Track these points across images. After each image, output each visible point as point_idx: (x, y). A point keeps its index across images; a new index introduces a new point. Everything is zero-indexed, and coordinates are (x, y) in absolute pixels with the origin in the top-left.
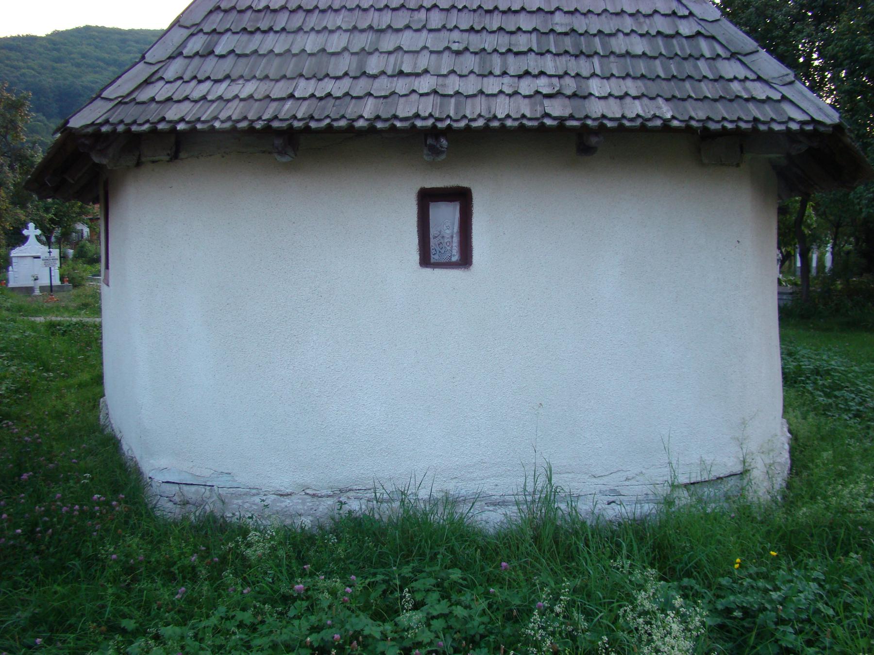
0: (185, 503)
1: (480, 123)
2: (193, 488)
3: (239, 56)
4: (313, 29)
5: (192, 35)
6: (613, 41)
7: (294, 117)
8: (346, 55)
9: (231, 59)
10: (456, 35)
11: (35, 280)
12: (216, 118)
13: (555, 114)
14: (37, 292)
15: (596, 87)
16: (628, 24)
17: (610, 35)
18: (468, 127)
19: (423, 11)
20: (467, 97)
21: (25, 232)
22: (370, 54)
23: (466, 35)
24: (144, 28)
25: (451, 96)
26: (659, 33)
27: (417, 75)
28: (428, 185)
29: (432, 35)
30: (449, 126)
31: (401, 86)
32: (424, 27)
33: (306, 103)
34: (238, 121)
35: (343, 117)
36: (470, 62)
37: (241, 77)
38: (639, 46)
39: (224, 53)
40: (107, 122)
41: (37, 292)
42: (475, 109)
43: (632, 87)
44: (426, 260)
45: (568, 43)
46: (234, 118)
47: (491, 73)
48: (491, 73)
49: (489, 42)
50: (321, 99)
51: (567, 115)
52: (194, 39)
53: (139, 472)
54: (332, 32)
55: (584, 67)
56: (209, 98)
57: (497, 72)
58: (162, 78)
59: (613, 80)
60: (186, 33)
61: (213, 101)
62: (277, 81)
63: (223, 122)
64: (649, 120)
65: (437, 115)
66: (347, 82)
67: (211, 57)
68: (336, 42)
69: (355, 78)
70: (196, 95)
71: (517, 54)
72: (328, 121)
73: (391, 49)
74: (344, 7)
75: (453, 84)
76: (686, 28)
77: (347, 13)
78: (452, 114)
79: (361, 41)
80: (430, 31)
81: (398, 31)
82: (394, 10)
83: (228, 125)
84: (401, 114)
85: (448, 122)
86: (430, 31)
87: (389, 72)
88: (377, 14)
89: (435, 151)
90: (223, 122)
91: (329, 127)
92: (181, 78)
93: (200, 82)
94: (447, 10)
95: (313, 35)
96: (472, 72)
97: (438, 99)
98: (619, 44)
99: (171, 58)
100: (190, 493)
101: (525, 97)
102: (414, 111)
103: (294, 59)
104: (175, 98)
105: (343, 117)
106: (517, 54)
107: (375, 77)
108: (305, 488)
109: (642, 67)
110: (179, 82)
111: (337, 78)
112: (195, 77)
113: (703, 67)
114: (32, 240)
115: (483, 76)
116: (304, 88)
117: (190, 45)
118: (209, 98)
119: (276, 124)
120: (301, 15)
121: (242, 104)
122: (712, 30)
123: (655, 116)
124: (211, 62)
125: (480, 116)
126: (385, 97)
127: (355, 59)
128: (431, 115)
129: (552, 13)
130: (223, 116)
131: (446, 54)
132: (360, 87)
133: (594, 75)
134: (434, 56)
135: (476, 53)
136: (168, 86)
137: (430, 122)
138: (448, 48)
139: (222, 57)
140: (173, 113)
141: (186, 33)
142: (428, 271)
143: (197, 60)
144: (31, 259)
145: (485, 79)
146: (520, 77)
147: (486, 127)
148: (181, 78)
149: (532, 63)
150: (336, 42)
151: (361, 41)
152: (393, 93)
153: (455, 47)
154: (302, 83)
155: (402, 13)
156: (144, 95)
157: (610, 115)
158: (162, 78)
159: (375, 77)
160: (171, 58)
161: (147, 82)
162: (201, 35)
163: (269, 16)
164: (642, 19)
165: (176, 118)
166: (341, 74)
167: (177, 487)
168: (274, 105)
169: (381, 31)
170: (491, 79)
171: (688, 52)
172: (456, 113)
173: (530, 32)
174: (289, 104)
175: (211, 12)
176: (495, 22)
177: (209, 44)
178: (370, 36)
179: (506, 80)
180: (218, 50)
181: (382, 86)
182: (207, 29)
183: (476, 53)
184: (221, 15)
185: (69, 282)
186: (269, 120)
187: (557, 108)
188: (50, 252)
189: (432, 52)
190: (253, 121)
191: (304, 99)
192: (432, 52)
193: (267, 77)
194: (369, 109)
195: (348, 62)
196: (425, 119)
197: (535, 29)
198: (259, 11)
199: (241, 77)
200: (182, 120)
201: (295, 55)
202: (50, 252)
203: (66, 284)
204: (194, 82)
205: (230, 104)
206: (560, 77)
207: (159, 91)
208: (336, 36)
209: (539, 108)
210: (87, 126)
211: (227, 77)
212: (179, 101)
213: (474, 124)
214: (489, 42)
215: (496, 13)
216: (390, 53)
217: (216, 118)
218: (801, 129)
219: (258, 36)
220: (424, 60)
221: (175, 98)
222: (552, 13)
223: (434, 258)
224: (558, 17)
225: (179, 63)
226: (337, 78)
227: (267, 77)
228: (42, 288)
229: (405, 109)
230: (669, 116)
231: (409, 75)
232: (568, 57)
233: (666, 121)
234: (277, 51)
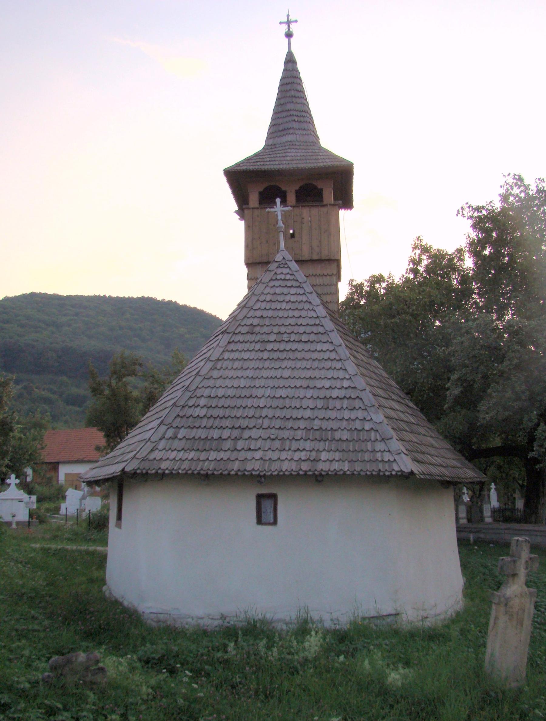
0: (159, 621)
1: (276, 473)
2: (162, 615)
3: (187, 439)
4: (217, 427)
5: (168, 428)
6: (336, 433)
7: (209, 469)
8: (229, 440)
9: (184, 441)
10: (273, 431)
11: (13, 516)
12: (180, 469)
13: (304, 469)
14: (14, 526)
15: (324, 456)
16: (344, 424)
17: (335, 430)
18: (271, 474)
19: (261, 419)
20: (274, 461)
21: (8, 481)
22: (239, 439)
23: (277, 430)
24: (74, 294)
25: (267, 460)
26: (356, 429)
27: (256, 450)
28: (260, 492)
29: (264, 431)
30: (265, 474)
31: (249, 455)
32: (261, 427)
33: (213, 462)
34: (188, 470)
35: (226, 470)
36: (277, 444)
37: (189, 449)
38: (345, 435)
39: (181, 438)
40: (139, 468)
41: (14, 526)
42: (275, 466)
43: (337, 456)
44: (260, 521)
45: (317, 435)
46: (187, 469)
47: (284, 449)
48: (284, 449)
49: (286, 434)
50: (219, 461)
51: (308, 470)
52: (169, 430)
53: (136, 611)
54: (224, 428)
55: (321, 446)
56: (177, 459)
57: (287, 449)
58: (157, 449)
59: (331, 452)
60: (166, 427)
61: (178, 461)
62: (202, 451)
63: (182, 470)
64: (338, 471)
65: (261, 470)
66: (229, 453)
67: (176, 439)
68: (226, 434)
69: (232, 451)
70: (171, 457)
71: (297, 440)
72: (221, 471)
73: (247, 438)
74: (230, 416)
75: (270, 454)
76: (367, 426)
77: (231, 419)
78: (266, 469)
79: (236, 433)
80: (264, 429)
81: (250, 428)
82: (250, 418)
83: (184, 472)
84: (248, 469)
85: (264, 472)
86: (264, 429)
87: (245, 449)
88: (243, 420)
89: (260, 482)
90: (182, 470)
91: (221, 474)
92: (165, 449)
93: (172, 451)
94: (271, 418)
95: (216, 429)
96: (277, 449)
97: (262, 462)
98: (338, 435)
99: (160, 439)
100: (161, 617)
101: (295, 461)
102: (252, 468)
103: (209, 441)
104: (164, 458)
105: (226, 470)
106: (297, 440)
107: (240, 451)
108: (209, 615)
109: (344, 446)
110: (164, 451)
111: (225, 451)
112: (170, 449)
113: (369, 446)
114: (13, 487)
115: (281, 451)
116: (213, 455)
117: (168, 433)
118: (177, 459)
119: (202, 472)
120: (212, 420)
121: (189, 462)
122: (378, 427)
123: (341, 470)
124: (176, 442)
125: (276, 470)
126: (243, 460)
127: (233, 441)
128: (258, 469)
129: (314, 419)
130: (182, 468)
131: (269, 440)
132: (234, 455)
133: (324, 450)
134: (263, 441)
135: (280, 440)
136: (160, 452)
137: (257, 473)
138: (269, 437)
139: (180, 439)
140: (164, 465)
141: (166, 427)
142: (260, 527)
143: (170, 441)
144: (17, 501)
145: (282, 452)
146: (295, 451)
147: (278, 475)
148: (165, 449)
149: (301, 444)
150: (226, 434)
151: (236, 433)
152: (246, 459)
153: (272, 437)
154: (212, 452)
155: (253, 420)
156: (151, 457)
157: (324, 470)
158: (157, 449)
159: (240, 451)
160: (160, 439)
161: (152, 450)
162: (171, 428)
163: (199, 420)
164: (351, 422)
165: (165, 468)
166: (227, 449)
167: (155, 615)
168: (201, 463)
169: (243, 429)
170: (284, 452)
171: (365, 438)
172: (268, 468)
173: (303, 429)
174: (207, 463)
175: (175, 417)
176: (290, 424)
177: (175, 433)
178: (239, 431)
179: (290, 453)
180: (179, 436)
181: (242, 455)
182: (174, 426)
183: (280, 440)
184: (180, 419)
185: (37, 518)
186: (199, 470)
187: (305, 467)
188: (30, 498)
189: (263, 439)
190: (193, 471)
191: (212, 461)
192: (263, 439)
193: (198, 449)
194: (236, 466)
195: (230, 443)
196: (256, 471)
197: (305, 428)
198: (195, 417)
199: (189, 449)
200: (167, 469)
201: (209, 440)
202: (30, 498)
203: (34, 520)
204: (170, 451)
205: (184, 462)
206: (311, 451)
207: (157, 455)
208: (226, 430)
209: (299, 466)
210: (131, 470)
211: (183, 449)
212: (165, 460)
213: (274, 474)
214: (286, 434)
215: (291, 419)
216: (246, 439)
217: (180, 469)
218: (396, 474)
219: (195, 430)
220: (259, 443)
221: (164, 458)
222: (314, 419)
223: (263, 520)
224: (316, 422)
225: (163, 442)
226: (225, 451)
227: (198, 449)
228: (18, 523)
229: (249, 467)
230: (346, 470)
231: (253, 450)
232: (316, 441)
233: (345, 472)
234: (202, 438)
